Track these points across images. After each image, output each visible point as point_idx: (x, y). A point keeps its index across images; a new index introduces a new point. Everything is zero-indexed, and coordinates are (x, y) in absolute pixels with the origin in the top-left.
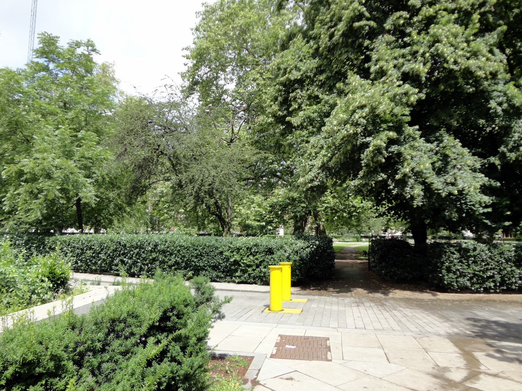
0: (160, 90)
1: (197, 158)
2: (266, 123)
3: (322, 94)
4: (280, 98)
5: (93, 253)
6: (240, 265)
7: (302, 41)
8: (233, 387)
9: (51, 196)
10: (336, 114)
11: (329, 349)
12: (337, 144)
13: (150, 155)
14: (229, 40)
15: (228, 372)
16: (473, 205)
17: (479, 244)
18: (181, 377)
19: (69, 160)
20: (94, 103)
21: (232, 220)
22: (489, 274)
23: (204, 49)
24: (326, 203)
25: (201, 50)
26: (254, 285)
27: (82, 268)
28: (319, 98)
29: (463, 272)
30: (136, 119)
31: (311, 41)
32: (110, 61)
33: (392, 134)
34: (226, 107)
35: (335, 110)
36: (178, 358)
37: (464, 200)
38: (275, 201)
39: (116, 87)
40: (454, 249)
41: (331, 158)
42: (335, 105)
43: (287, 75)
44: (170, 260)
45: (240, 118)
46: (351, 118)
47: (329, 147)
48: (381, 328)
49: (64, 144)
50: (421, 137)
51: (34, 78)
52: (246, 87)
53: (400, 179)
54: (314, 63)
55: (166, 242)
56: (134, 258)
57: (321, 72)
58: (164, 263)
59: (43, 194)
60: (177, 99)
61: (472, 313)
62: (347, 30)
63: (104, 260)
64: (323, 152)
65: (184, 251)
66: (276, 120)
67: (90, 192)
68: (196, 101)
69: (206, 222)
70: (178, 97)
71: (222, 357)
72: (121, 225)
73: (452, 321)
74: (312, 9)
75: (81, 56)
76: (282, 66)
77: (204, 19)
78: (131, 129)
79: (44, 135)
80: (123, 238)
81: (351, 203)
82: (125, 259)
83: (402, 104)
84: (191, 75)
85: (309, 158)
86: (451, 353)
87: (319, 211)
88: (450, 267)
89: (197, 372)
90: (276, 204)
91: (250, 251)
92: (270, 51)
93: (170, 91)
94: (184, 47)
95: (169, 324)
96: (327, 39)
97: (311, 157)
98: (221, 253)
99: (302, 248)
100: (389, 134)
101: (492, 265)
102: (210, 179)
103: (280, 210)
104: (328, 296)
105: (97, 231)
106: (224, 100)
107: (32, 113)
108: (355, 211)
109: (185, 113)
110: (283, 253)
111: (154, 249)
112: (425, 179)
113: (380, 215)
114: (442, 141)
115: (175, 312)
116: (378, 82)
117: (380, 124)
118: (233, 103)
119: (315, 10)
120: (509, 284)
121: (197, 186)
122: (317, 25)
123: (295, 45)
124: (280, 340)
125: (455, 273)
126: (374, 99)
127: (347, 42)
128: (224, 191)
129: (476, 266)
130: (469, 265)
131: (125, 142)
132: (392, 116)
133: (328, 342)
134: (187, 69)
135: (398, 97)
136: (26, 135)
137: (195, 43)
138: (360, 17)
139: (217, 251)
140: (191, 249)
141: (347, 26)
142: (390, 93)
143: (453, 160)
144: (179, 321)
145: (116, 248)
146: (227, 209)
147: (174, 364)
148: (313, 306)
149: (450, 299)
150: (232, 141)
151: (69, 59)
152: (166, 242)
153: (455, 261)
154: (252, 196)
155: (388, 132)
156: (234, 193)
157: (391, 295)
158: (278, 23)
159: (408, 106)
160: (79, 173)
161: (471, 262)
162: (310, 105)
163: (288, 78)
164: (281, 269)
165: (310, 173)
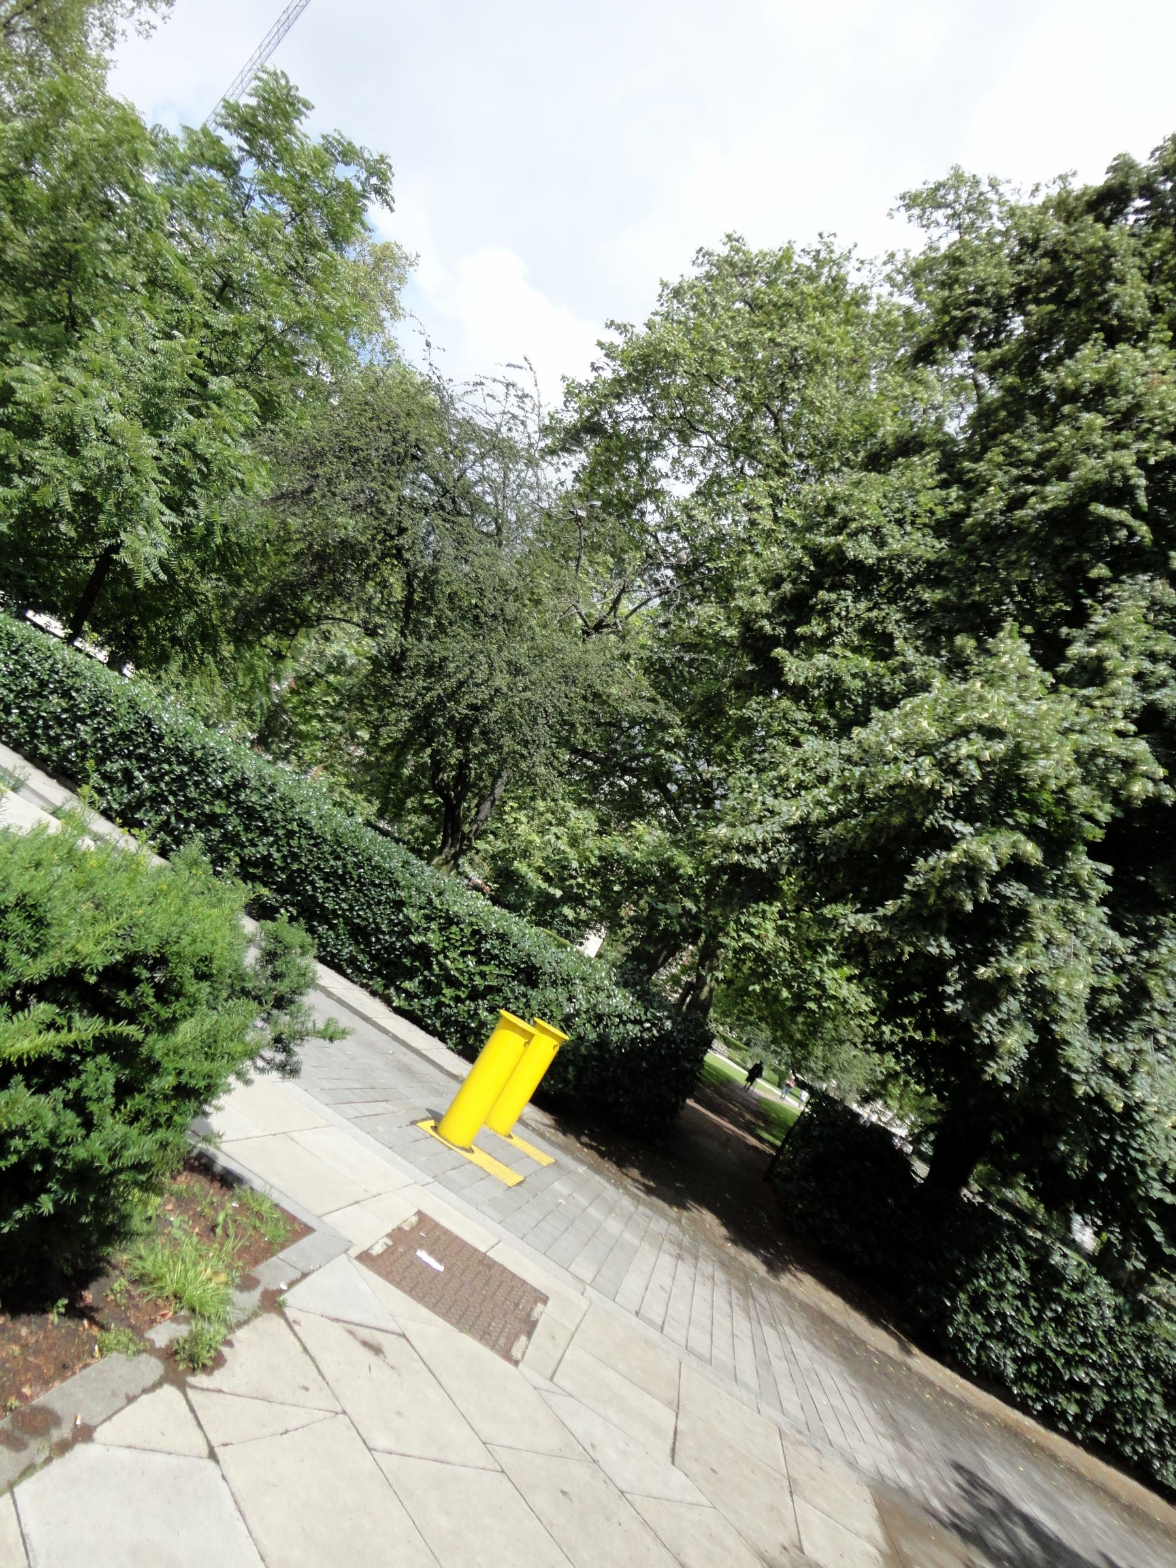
0: (490, 387)
1: (483, 619)
2: (717, 634)
3: (905, 639)
4: (787, 587)
5: (64, 711)
6: (428, 966)
7: (931, 475)
8: (204, 1277)
9: (44, 497)
10: (913, 711)
11: (530, 1327)
12: (871, 792)
13: (363, 540)
14: (743, 367)
15: (219, 1231)
16: (1143, 1165)
17: (1098, 1279)
18: (70, 1167)
19: (146, 432)
20: (304, 326)
21: (481, 835)
22: (1081, 1374)
23: (666, 354)
24: (752, 934)
25: (658, 351)
26: (435, 1042)
27: (14, 733)
28: (891, 646)
29: (1012, 1330)
30: (385, 427)
31: (955, 488)
32: (409, 249)
33: (1031, 850)
34: (636, 535)
35: (916, 700)
36: (93, 1107)
37: (1123, 1135)
38: (623, 850)
39: (386, 324)
40: (1024, 1254)
41: (832, 821)
42: (925, 687)
43: (841, 538)
44: (255, 845)
45: (657, 583)
46: (945, 744)
47: (845, 789)
48: (706, 1352)
49: (160, 384)
50: (1102, 902)
51: (187, 173)
52: (719, 513)
53: (984, 982)
54: (929, 547)
55: (272, 790)
56: (163, 785)
57: (938, 582)
58: (234, 844)
59: (29, 480)
60: (518, 437)
61: (975, 1454)
62: (1065, 509)
63: (83, 745)
64: (822, 793)
65: (303, 842)
66: (743, 638)
67: (154, 545)
68: (567, 475)
69: (410, 803)
70: (527, 434)
71: (228, 1180)
72: (183, 681)
73: (908, 1446)
74: (1003, 405)
75: (340, 185)
76: (842, 509)
77: (709, 277)
78: (355, 444)
79: (121, 332)
80: (166, 716)
81: (817, 973)
82: (137, 774)
83: (1100, 787)
84: (593, 402)
85: (773, 787)
86: (857, 1534)
87: (724, 946)
88: (985, 1295)
89: (122, 1177)
90: (621, 860)
91: (479, 943)
92: (835, 456)
93: (512, 406)
94: (618, 321)
95: (123, 998)
96: (1000, 505)
97: (779, 788)
98: (399, 905)
99: (620, 1016)
100: (1021, 846)
101: (1101, 1356)
102: (483, 694)
103: (622, 883)
104: (615, 1185)
105: (115, 663)
106: (643, 514)
107: (126, 260)
108: (817, 1000)
109: (520, 486)
110: (562, 999)
111: (230, 792)
112: (1054, 1020)
113: (881, 1047)
114: (1152, 945)
115: (158, 976)
116: (1070, 691)
117: (1013, 806)
118: (659, 535)
119: (1010, 414)
120: (1119, 1434)
121: (438, 690)
122: (995, 454)
123: (908, 473)
124: (413, 1229)
125: (989, 1320)
126: (1035, 732)
127: (1048, 541)
128: (501, 747)
129: (1057, 1335)
130: (1038, 1321)
131: (320, 471)
132: (1058, 802)
133: (540, 1306)
134: (592, 380)
135: (1100, 761)
136: (76, 307)
137: (650, 326)
138: (1120, 495)
139: (391, 895)
140: (326, 848)
141: (1070, 499)
142: (1085, 739)
143: (1155, 1014)
144: (156, 1007)
145: (132, 732)
146: (483, 799)
147: (71, 1117)
148: (557, 1186)
149: (937, 1381)
150: (599, 626)
151: (304, 177)
152: (272, 790)
153: (1010, 1287)
154: (570, 806)
155: (1023, 838)
156: (524, 765)
157: (786, 1280)
158: (896, 398)
159: (1116, 801)
160: (154, 479)
161: (1049, 1314)
162: (857, 650)
163: (839, 546)
164: (529, 1037)
165: (753, 826)
